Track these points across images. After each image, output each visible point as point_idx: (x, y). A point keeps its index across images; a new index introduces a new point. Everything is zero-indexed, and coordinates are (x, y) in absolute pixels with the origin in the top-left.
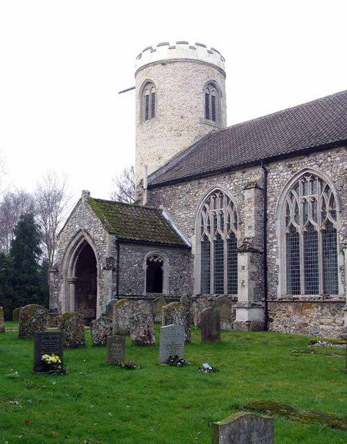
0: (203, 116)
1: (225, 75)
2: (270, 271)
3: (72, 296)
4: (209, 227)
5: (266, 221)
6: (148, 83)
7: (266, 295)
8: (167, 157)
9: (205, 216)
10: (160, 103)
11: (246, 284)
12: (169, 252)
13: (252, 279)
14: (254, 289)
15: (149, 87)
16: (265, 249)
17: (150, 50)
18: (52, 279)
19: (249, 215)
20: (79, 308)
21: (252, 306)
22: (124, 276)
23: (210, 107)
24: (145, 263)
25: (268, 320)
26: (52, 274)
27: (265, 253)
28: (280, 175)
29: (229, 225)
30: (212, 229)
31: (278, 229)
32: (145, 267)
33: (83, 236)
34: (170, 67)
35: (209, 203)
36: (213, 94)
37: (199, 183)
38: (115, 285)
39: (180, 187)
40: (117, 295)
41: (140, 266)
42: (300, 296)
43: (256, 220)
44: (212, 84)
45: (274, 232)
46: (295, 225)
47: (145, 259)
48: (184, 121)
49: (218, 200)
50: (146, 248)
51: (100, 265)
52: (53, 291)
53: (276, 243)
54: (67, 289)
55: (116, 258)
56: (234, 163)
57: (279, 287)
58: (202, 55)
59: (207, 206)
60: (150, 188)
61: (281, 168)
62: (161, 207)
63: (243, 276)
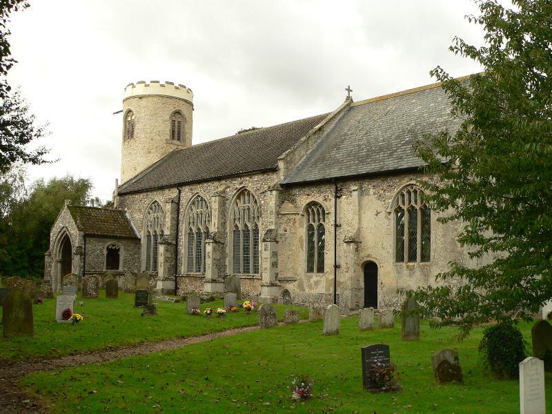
0: (168, 138)
1: (192, 105)
3: (59, 271)
5: (178, 224)
6: (130, 111)
7: (176, 272)
8: (140, 169)
9: (236, 209)
10: (138, 128)
12: (125, 242)
14: (168, 268)
15: (130, 114)
16: (177, 242)
17: (131, 86)
18: (46, 260)
19: (168, 222)
21: (166, 279)
22: (89, 259)
23: (176, 131)
25: (177, 288)
26: (46, 257)
27: (177, 245)
28: (187, 193)
30: (196, 223)
31: (183, 227)
32: (105, 252)
33: (65, 231)
34: (144, 101)
35: (151, 209)
38: (82, 264)
42: (192, 273)
43: (171, 223)
50: (106, 240)
51: (74, 251)
54: (56, 267)
55: (83, 247)
58: (169, 91)
60: (120, 194)
62: (126, 209)
63: (161, 259)
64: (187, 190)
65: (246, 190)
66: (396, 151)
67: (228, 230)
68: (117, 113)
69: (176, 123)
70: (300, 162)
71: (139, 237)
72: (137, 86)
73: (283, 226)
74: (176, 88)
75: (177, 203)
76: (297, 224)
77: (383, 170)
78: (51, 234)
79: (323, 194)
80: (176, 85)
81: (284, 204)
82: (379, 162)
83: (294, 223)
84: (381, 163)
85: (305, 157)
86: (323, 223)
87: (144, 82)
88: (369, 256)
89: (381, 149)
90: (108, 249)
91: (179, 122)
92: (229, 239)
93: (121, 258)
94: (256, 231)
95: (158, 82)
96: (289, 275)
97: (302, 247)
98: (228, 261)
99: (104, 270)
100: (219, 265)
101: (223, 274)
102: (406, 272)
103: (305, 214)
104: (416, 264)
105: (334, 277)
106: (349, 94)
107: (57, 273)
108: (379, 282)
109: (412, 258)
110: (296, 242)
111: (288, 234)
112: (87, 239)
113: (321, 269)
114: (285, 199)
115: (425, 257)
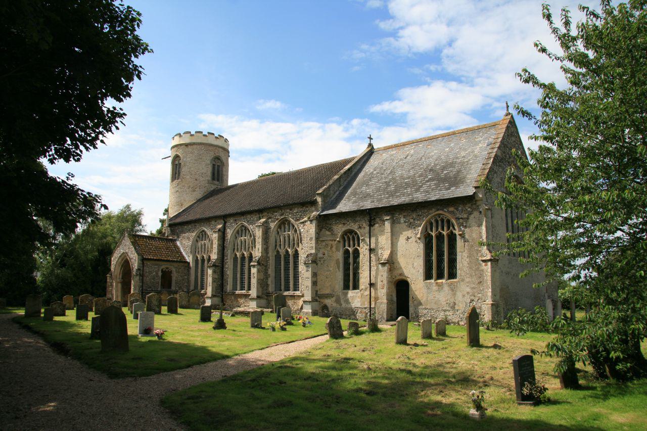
0: (210, 179)
2: (225, 277)
4: (280, 245)
11: (211, 284)
13: (215, 282)
15: (178, 159)
20: (124, 297)
24: (160, 272)
29: (294, 244)
32: (160, 274)
36: (218, 164)
37: (195, 226)
38: (141, 284)
39: (186, 227)
40: (142, 290)
41: (157, 273)
44: (218, 158)
45: (227, 256)
46: (280, 250)
47: (160, 270)
48: (198, 182)
49: (204, 235)
52: (109, 287)
53: (228, 262)
54: (117, 286)
55: (142, 269)
56: (211, 215)
57: (228, 286)
58: (211, 140)
59: (198, 239)
61: (232, 221)
64: (232, 221)
65: (287, 220)
66: (421, 186)
67: (270, 254)
68: (165, 158)
69: (216, 166)
70: (334, 197)
71: (188, 261)
72: (184, 136)
73: (322, 251)
74: (216, 138)
75: (223, 233)
76: (334, 249)
77: (414, 202)
78: (112, 259)
79: (357, 224)
80: (216, 135)
81: (322, 232)
82: (409, 196)
83: (331, 248)
84: (410, 196)
85: (337, 193)
86: (358, 248)
87: (190, 132)
88: (401, 275)
89: (408, 185)
90: (162, 270)
91: (218, 166)
92: (272, 262)
93: (174, 279)
94: (296, 255)
95: (202, 132)
96: (327, 291)
97: (339, 268)
98: (271, 281)
99: (159, 289)
100: (262, 284)
101: (265, 292)
102: (435, 288)
103: (341, 241)
104: (444, 281)
105: (369, 293)
106: (370, 141)
107: (527, 403)
108: (310, 291)
109: (440, 276)
110: (333, 264)
111: (326, 257)
112: (145, 262)
113: (356, 287)
114: (322, 228)
115: (452, 275)
